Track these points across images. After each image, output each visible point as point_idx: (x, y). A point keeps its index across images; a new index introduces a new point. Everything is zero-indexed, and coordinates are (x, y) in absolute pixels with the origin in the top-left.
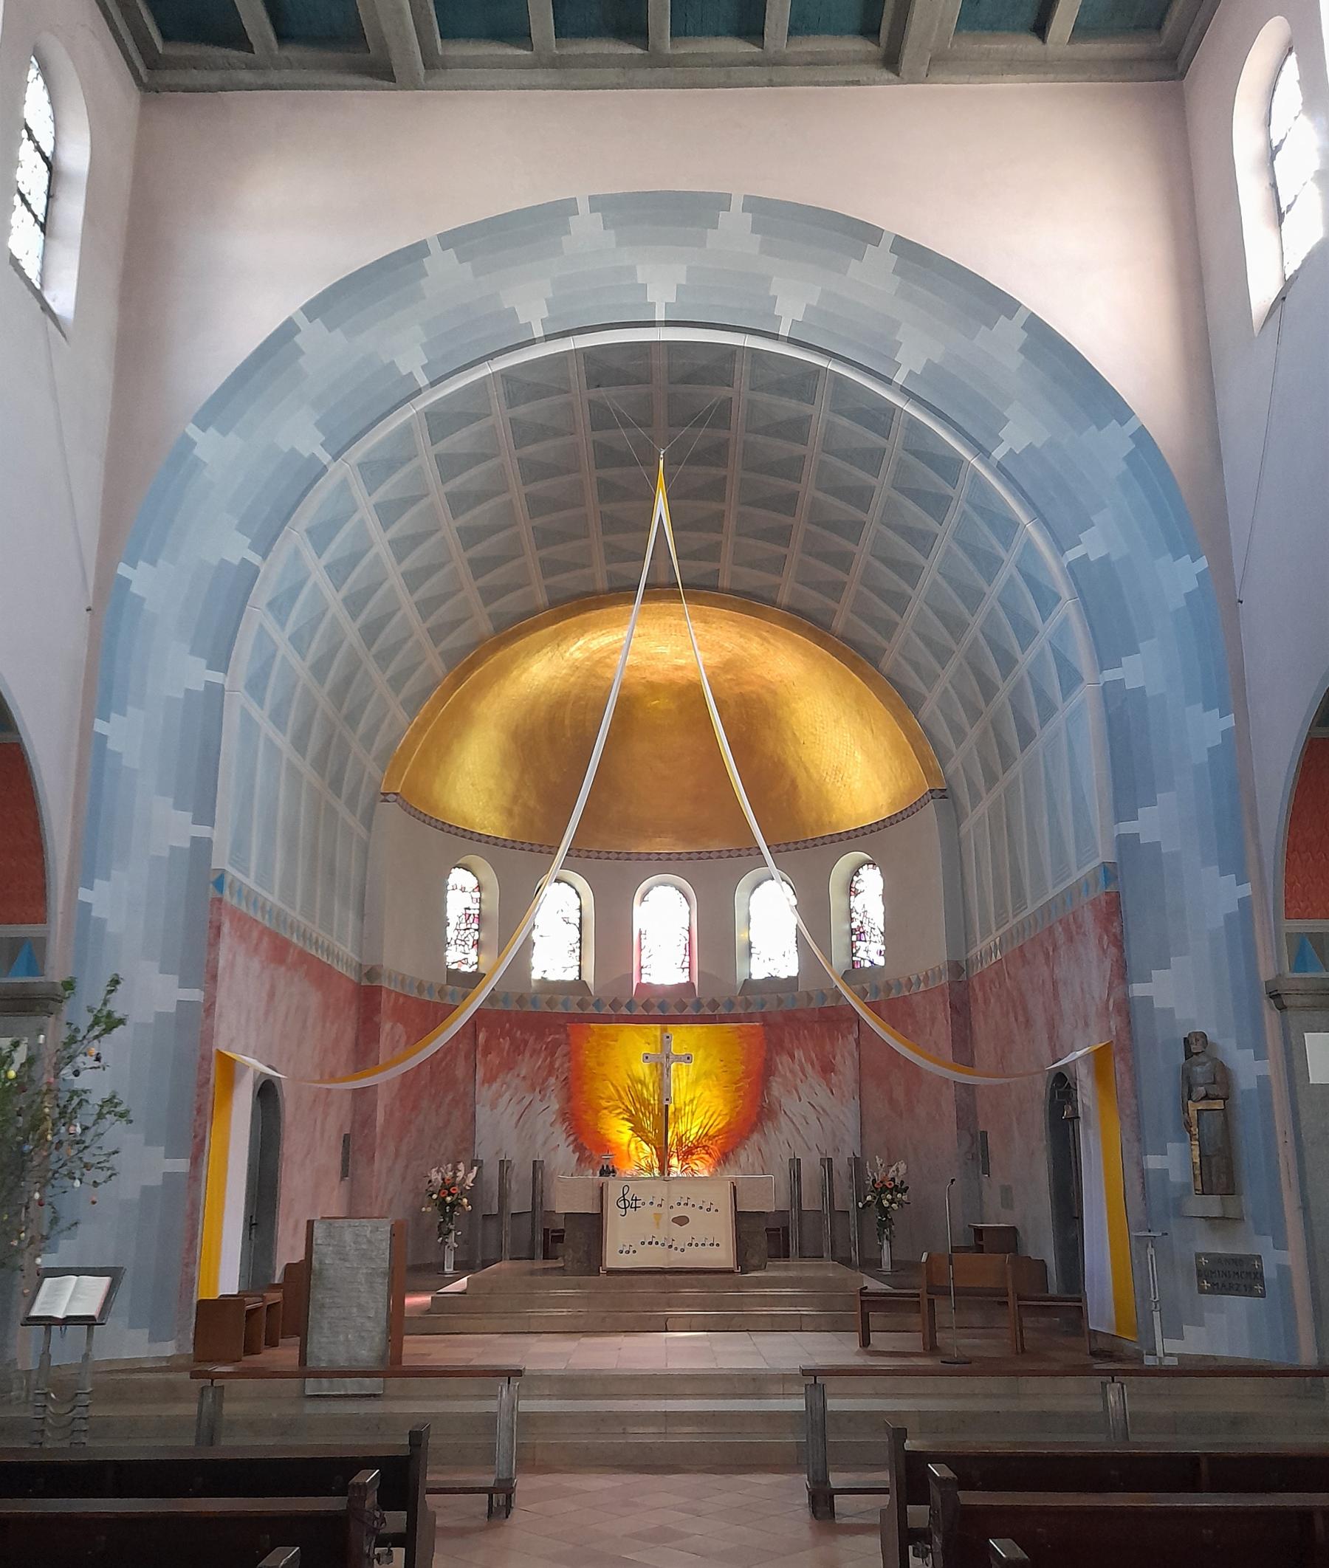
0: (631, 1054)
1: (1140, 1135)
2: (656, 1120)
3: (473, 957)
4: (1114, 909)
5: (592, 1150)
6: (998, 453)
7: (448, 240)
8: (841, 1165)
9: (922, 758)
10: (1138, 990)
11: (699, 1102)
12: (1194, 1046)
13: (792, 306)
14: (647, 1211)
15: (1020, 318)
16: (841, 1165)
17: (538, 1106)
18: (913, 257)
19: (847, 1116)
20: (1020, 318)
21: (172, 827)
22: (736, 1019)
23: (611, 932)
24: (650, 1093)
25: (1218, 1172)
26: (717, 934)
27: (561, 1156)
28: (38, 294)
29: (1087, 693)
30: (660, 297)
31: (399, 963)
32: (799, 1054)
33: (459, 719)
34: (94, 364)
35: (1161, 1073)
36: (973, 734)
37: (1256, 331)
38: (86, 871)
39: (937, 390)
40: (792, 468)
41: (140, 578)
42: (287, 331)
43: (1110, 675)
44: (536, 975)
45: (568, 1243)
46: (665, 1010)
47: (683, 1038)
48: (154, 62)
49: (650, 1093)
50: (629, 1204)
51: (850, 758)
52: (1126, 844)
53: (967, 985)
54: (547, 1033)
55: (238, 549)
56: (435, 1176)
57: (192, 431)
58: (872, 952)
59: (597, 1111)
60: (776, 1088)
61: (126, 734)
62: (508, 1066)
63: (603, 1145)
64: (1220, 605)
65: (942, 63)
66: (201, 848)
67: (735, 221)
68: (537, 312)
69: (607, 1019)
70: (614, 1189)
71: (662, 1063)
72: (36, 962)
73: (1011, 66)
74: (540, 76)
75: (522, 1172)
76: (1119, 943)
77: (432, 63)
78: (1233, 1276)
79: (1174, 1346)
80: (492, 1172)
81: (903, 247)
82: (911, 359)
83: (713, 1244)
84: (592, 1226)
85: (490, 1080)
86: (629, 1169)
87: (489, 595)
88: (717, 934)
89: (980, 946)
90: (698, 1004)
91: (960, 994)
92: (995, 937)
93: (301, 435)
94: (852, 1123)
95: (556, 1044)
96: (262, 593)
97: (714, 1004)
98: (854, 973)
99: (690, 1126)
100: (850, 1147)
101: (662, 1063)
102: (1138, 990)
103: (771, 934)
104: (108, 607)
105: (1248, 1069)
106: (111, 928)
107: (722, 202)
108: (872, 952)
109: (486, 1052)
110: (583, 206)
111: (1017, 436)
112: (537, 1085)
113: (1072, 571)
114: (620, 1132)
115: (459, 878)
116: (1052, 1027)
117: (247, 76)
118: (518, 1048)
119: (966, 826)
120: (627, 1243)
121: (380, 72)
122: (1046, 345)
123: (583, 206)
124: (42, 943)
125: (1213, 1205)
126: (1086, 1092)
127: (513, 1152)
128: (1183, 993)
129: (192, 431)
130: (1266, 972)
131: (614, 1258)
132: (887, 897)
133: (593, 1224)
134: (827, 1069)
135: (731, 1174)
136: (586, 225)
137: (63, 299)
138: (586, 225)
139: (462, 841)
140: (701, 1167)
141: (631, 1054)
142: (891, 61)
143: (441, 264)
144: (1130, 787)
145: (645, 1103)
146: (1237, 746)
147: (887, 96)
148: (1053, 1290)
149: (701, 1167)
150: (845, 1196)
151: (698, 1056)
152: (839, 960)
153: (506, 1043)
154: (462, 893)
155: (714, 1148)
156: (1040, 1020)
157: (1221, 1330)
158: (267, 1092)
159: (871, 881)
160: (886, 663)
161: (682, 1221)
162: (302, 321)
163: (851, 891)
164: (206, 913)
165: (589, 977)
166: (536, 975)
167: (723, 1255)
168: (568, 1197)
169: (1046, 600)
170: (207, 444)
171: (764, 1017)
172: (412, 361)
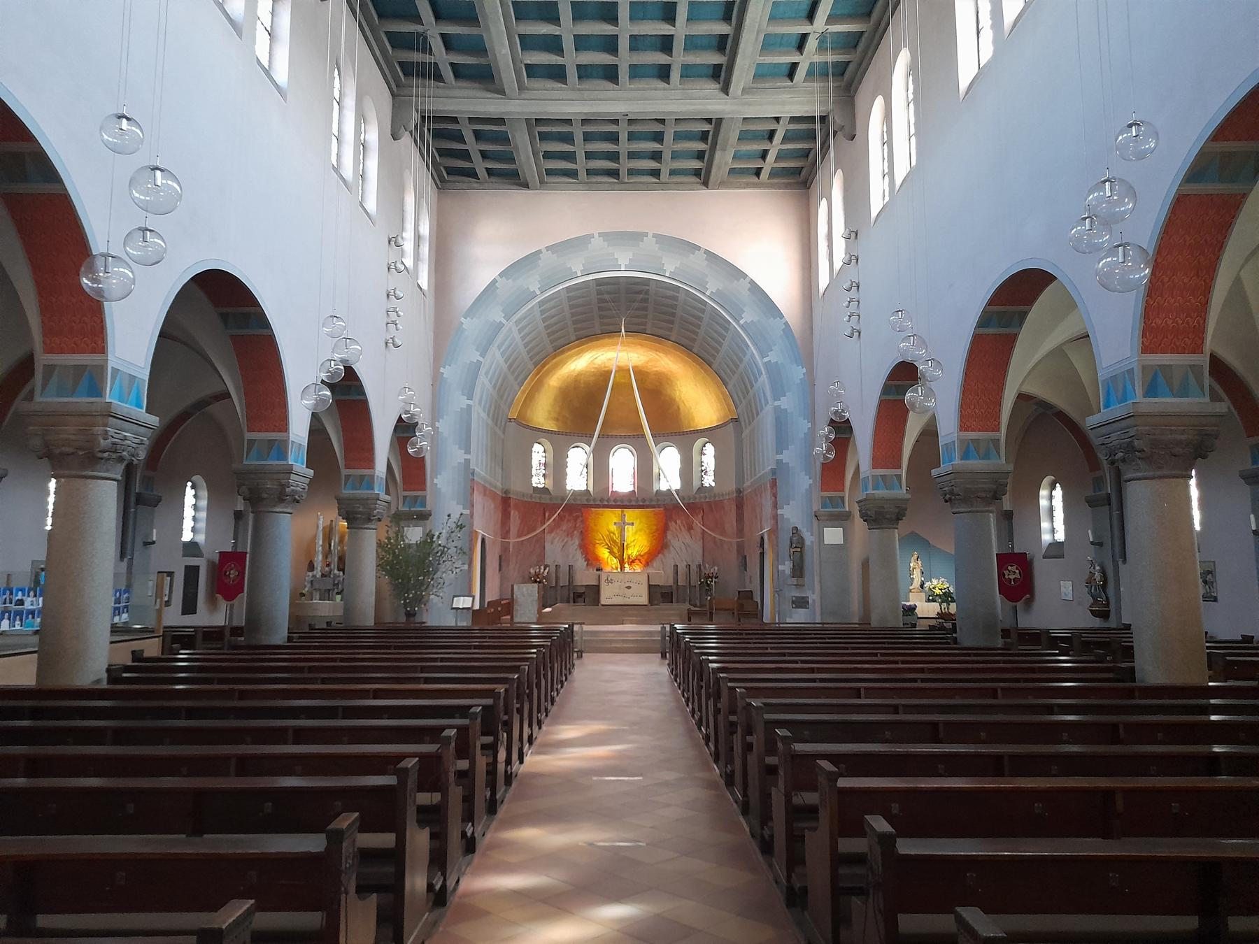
0: (608, 521)
1: (777, 560)
2: (619, 549)
3: (542, 480)
5: (592, 561)
6: (742, 322)
7: (548, 248)
8: (694, 568)
9: (728, 405)
11: (637, 540)
13: (669, 270)
14: (616, 584)
15: (747, 280)
16: (694, 568)
18: (712, 257)
19: (697, 548)
20: (747, 280)
21: (458, 456)
23: (600, 468)
24: (616, 537)
26: (645, 470)
27: (580, 563)
28: (267, 72)
30: (624, 264)
31: (516, 487)
32: (679, 522)
33: (537, 386)
34: (430, 301)
35: (785, 537)
37: (961, 96)
38: (434, 476)
39: (719, 296)
40: (674, 307)
41: (446, 371)
42: (495, 281)
43: (776, 403)
45: (588, 596)
46: (623, 503)
47: (630, 515)
48: (442, 180)
49: (616, 537)
50: (609, 581)
51: (700, 402)
52: (779, 462)
54: (577, 512)
55: (476, 356)
56: (532, 571)
57: (463, 319)
58: (709, 481)
60: (669, 537)
61: (444, 426)
63: (597, 559)
64: (810, 383)
65: (722, 184)
66: (467, 461)
67: (649, 241)
68: (580, 271)
69: (598, 506)
70: (604, 578)
71: (622, 526)
72: (423, 504)
73: (747, 186)
74: (580, 186)
75: (564, 569)
76: (775, 496)
77: (521, 88)
78: (801, 603)
79: (41, 400)
80: (553, 569)
81: (707, 252)
82: (712, 288)
83: (640, 596)
86: (607, 569)
87: (552, 342)
88: (645, 470)
89: (747, 484)
93: (496, 315)
94: (700, 551)
95: (577, 517)
96: (483, 371)
97: (644, 500)
98: (702, 488)
99: (633, 551)
100: (699, 560)
101: (622, 526)
102: (780, 512)
103: (669, 468)
104: (437, 381)
105: (809, 539)
106: (443, 490)
107: (646, 235)
108: (709, 481)
110: (596, 236)
111: (747, 317)
112: (570, 534)
113: (766, 365)
114: (604, 553)
115: (537, 448)
117: (476, 185)
120: (608, 595)
121: (526, 186)
122: (755, 288)
123: (596, 236)
124: (425, 497)
125: (794, 581)
127: (560, 561)
128: (793, 514)
129: (463, 319)
131: (603, 601)
133: (596, 589)
135: (650, 570)
136: (597, 242)
137: (281, 73)
138: (597, 242)
139: (538, 433)
140: (638, 568)
141: (608, 521)
142: (706, 184)
143: (546, 255)
144: (781, 445)
145: (614, 542)
146: (813, 430)
147: (704, 192)
149: (638, 568)
150: (695, 581)
151: (637, 523)
152: (696, 484)
154: (538, 454)
155: (643, 561)
157: (798, 617)
158: (483, 540)
159: (710, 450)
160: (715, 366)
161: (629, 588)
162: (499, 279)
163: (702, 453)
164: (470, 484)
165: (591, 489)
166: (568, 488)
167: (644, 600)
168: (584, 577)
170: (466, 323)
172: (534, 287)
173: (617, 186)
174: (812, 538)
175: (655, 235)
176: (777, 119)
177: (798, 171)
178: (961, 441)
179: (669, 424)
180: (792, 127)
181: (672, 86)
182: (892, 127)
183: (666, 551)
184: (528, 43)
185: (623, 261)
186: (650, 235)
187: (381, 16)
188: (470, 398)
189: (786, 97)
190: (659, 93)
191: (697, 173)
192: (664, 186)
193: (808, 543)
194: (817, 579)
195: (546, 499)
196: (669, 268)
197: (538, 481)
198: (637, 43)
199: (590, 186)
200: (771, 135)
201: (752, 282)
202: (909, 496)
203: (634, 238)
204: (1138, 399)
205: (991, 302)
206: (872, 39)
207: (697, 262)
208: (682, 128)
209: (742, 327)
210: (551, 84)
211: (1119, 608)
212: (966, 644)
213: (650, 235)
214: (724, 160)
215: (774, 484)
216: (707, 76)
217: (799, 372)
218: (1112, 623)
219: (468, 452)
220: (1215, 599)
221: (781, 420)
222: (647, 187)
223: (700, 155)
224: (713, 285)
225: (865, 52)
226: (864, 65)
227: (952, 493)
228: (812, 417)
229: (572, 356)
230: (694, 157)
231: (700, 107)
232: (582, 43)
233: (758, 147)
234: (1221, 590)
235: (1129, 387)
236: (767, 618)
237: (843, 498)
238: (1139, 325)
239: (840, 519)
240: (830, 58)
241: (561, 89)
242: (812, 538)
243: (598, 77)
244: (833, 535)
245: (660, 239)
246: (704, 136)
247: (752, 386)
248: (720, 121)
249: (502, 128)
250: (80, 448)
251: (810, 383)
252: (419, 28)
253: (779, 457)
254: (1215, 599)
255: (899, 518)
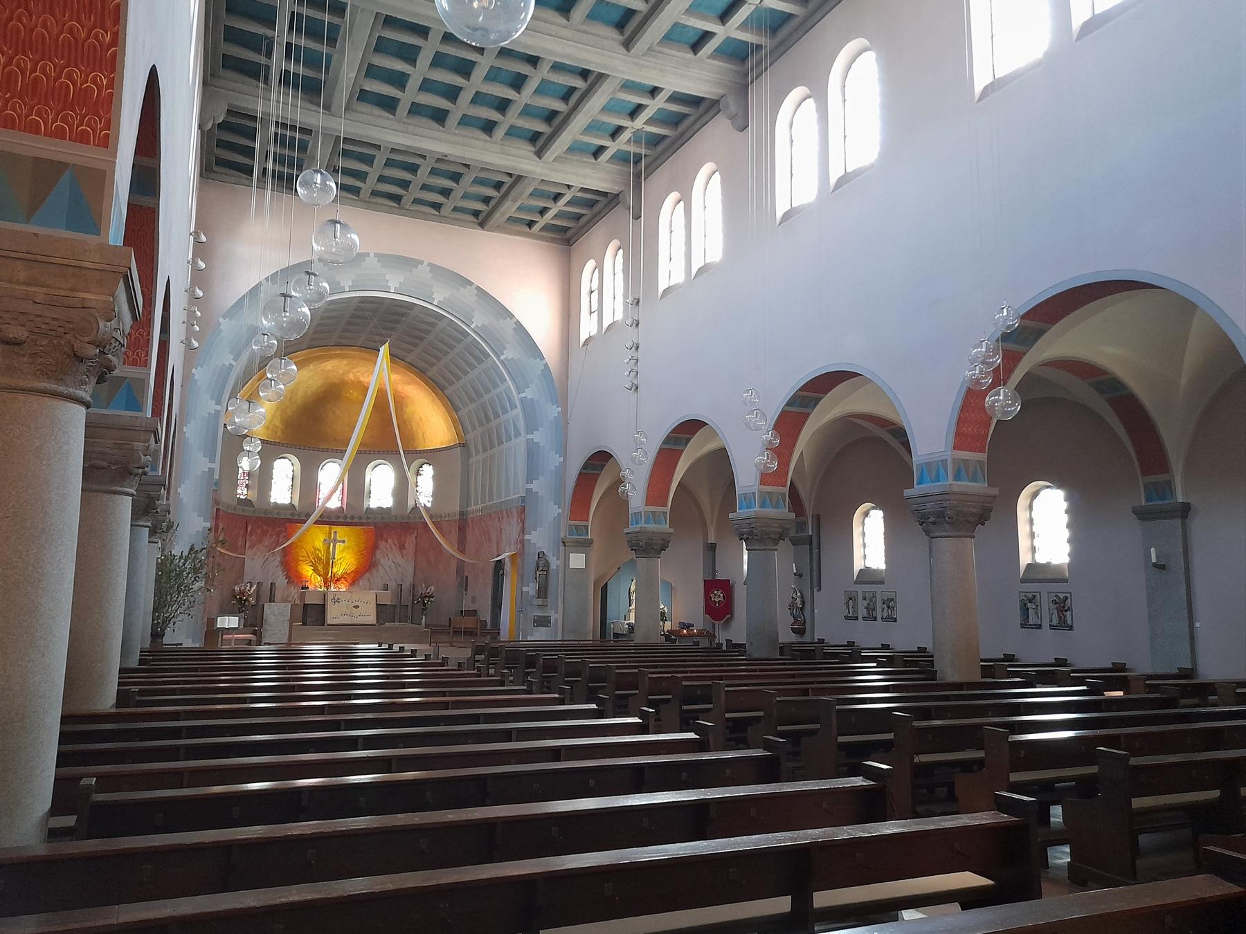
1: (522, 580)
2: (324, 565)
4: (523, 511)
6: (502, 358)
10: (527, 537)
11: (345, 560)
12: (541, 555)
13: (438, 298)
17: (271, 559)
18: (482, 294)
22: (362, 524)
23: (307, 483)
24: (322, 555)
25: (543, 592)
26: (355, 485)
29: (521, 440)
30: (393, 287)
35: (531, 560)
36: (479, 430)
39: (483, 332)
41: (197, 373)
42: (259, 285)
43: (530, 436)
44: (272, 500)
46: (329, 519)
47: (341, 532)
49: (322, 555)
50: (336, 601)
51: (433, 424)
52: (529, 491)
53: (465, 520)
54: (281, 523)
56: (237, 588)
57: (221, 320)
59: (297, 561)
60: (378, 554)
62: (260, 541)
64: (563, 424)
65: (499, 229)
68: (349, 286)
73: (518, 233)
78: (543, 622)
84: (321, 609)
85: (252, 547)
88: (355, 485)
89: (473, 508)
90: (346, 517)
91: (462, 526)
92: (479, 506)
94: (411, 570)
97: (353, 517)
99: (339, 569)
101: (330, 541)
102: (527, 537)
103: (381, 485)
105: (554, 563)
109: (251, 535)
111: (508, 354)
113: (522, 400)
114: (307, 571)
116: (498, 542)
118: (264, 533)
119: (471, 461)
122: (520, 328)
123: (372, 255)
125: (540, 601)
126: (508, 566)
127: (259, 578)
128: (539, 539)
129: (221, 320)
130: (562, 535)
131: (330, 620)
132: (435, 478)
134: (402, 547)
136: (371, 261)
138: (371, 261)
141: (316, 538)
142: (482, 225)
144: (532, 473)
145: (320, 559)
146: (564, 465)
147: (478, 232)
148: (489, 627)
150: (407, 598)
152: (411, 503)
153: (259, 531)
155: (349, 580)
156: (494, 538)
157: (540, 635)
161: (357, 607)
163: (418, 474)
165: (296, 503)
166: (272, 500)
167: (372, 619)
169: (513, 407)
170: (225, 324)
171: (375, 524)
173: (396, 211)
174: (558, 563)
175: (430, 264)
176: (569, 186)
177: (566, 229)
178: (761, 493)
179: (390, 440)
180: (579, 194)
181: (494, 139)
182: (691, 225)
183: (374, 570)
184: (372, 72)
185: (394, 284)
186: (426, 264)
187: (228, 10)
188: (218, 403)
189: (587, 171)
190: (480, 144)
191: (476, 214)
192: (444, 219)
193: (553, 566)
194: (560, 600)
195: (249, 512)
196: (438, 298)
197: (242, 492)
198: (478, 99)
199: (368, 205)
200: (557, 197)
201: (518, 323)
202: (672, 530)
203: (409, 263)
204: (948, 482)
205: (802, 389)
206: (673, 143)
207: (466, 297)
208: (483, 175)
209: (502, 362)
210: (377, 111)
211: (813, 630)
212: (756, 656)
213: (426, 264)
214: (510, 208)
215: (522, 511)
216: (525, 138)
217: (554, 411)
218: (807, 638)
219: (212, 460)
220: (895, 620)
221: (532, 452)
222: (426, 217)
223: (487, 200)
224: (479, 320)
225: (665, 151)
226: (658, 162)
227: (751, 533)
228: (563, 450)
229: (417, 383)
230: (484, 202)
231: (516, 165)
232: (427, 86)
233: (542, 204)
234: (900, 613)
235: (942, 472)
236: (504, 635)
237: (586, 527)
238: (953, 431)
239: (583, 545)
240: (632, 149)
241: (388, 119)
242: (558, 563)
243: (426, 116)
244: (577, 560)
245: (434, 268)
246: (498, 186)
247: (497, 416)
248: (520, 178)
249: (250, 124)
250: (116, 463)
251: (563, 424)
252: (269, 33)
253: (529, 486)
254: (895, 620)
255: (663, 549)
